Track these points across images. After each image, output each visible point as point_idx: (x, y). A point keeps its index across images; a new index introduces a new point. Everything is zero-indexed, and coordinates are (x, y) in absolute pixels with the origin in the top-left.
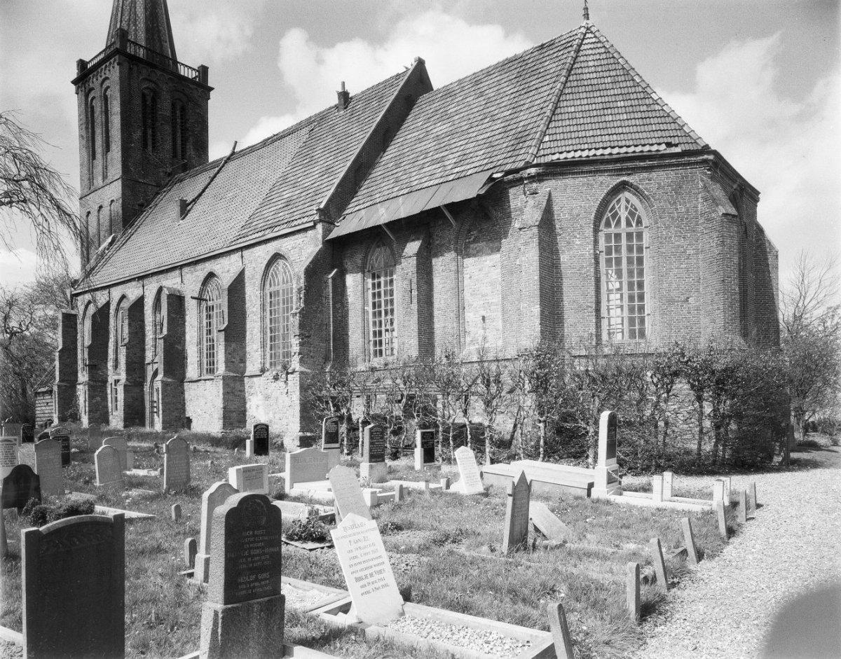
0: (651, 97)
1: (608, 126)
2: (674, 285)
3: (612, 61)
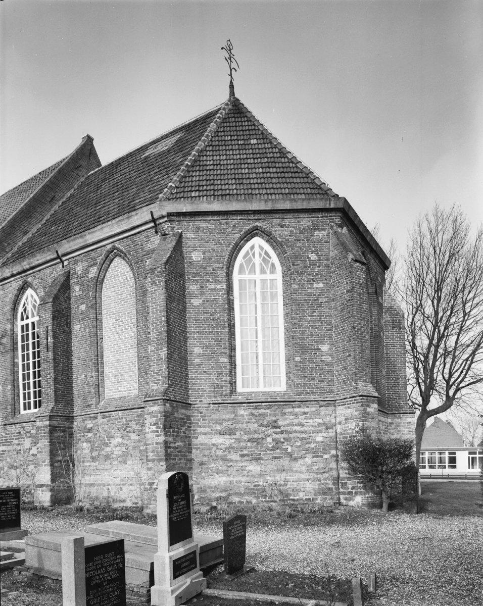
2: (307, 333)
3: (253, 127)
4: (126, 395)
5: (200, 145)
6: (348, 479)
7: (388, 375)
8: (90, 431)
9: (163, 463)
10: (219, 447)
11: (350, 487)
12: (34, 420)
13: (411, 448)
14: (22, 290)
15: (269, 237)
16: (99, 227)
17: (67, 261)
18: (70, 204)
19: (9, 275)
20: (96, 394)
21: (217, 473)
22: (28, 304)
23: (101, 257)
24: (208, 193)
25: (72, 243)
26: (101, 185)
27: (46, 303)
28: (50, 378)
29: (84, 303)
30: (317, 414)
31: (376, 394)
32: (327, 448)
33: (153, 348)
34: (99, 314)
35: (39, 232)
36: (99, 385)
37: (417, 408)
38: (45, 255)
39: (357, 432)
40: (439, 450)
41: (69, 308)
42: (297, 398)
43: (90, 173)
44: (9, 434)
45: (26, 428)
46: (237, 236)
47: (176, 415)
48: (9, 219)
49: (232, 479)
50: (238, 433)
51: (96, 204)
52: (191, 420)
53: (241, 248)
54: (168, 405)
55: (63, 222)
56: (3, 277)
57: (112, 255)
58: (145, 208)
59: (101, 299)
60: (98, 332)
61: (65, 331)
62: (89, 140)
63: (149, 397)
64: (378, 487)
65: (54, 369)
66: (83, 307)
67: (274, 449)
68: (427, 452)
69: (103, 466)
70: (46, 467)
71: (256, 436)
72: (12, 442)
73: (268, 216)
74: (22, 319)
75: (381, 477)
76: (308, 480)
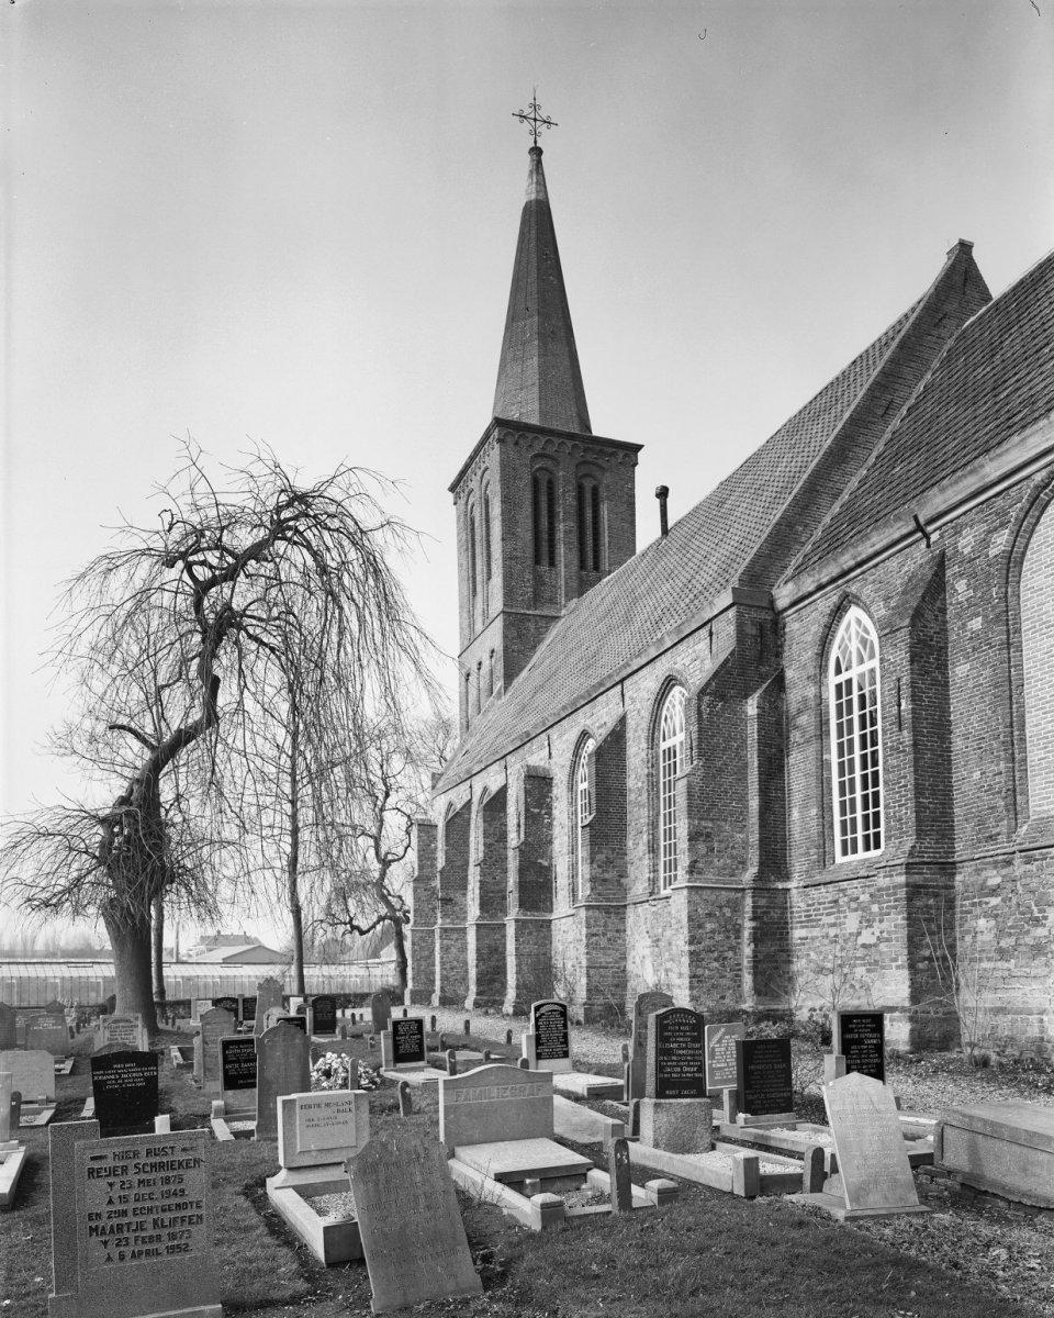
8: (994, 892)
12: (866, 875)
14: (838, 612)
16: (1016, 439)
17: (938, 532)
18: (929, 407)
19: (811, 588)
20: (1008, 810)
22: (850, 639)
23: (1019, 505)
25: (950, 492)
26: (1001, 342)
27: (897, 630)
28: (905, 786)
29: (978, 615)
34: (1014, 633)
35: (867, 485)
36: (1014, 791)
38: (888, 531)
41: (943, 631)
43: (968, 323)
44: (813, 904)
45: (849, 892)
48: (805, 476)
51: (994, 389)
55: (919, 450)
57: (1046, 494)
59: (1019, 597)
60: (1013, 673)
61: (935, 682)
62: (964, 248)
65: (915, 766)
66: (976, 624)
69: (1028, 970)
72: (820, 920)
74: (838, 671)
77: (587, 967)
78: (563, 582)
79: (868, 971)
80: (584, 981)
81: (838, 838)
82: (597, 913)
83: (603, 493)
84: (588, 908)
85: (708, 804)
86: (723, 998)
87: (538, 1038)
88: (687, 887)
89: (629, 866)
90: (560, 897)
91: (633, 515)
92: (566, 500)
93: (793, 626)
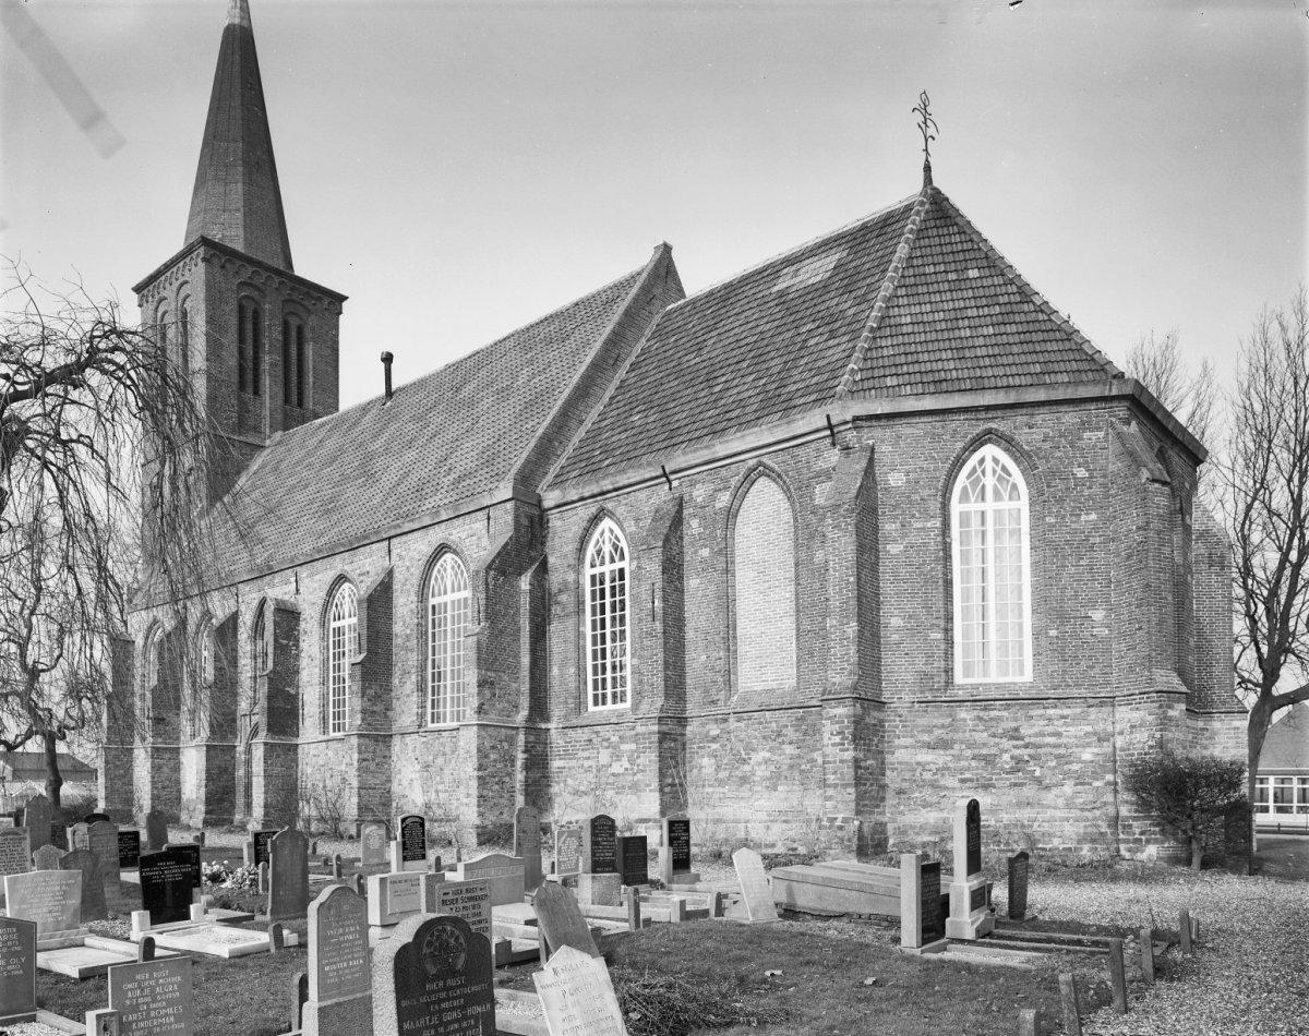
0: (1032, 301)
1: (919, 349)
2: (1069, 593)
3: (970, 245)
4: (775, 687)
5: (887, 287)
6: (1135, 819)
7: (1198, 647)
8: (714, 739)
9: (852, 790)
10: (927, 767)
11: (1138, 831)
13: (1241, 772)
14: (595, 520)
15: (1008, 443)
19: (575, 498)
21: (924, 807)
24: (913, 380)
25: (690, 456)
29: (706, 547)
30: (1083, 718)
31: (1184, 689)
32: (1099, 771)
33: (835, 622)
37: (1250, 689)
39: (1151, 747)
40: (1299, 773)
42: (1051, 694)
45: (601, 734)
46: (960, 445)
47: (867, 720)
49: (945, 815)
50: (956, 746)
52: (884, 726)
53: (964, 462)
54: (858, 705)
56: (565, 500)
58: (817, 411)
61: (676, 590)
63: (830, 693)
64: (1185, 832)
66: (705, 552)
67: (1013, 771)
68: (1272, 778)
70: (652, 794)
71: (984, 752)
73: (1009, 413)
75: (1189, 816)
76: (1067, 820)
77: (359, 788)
78: (268, 413)
79: (617, 793)
80: (355, 800)
81: (590, 692)
82: (367, 741)
83: (308, 334)
84: (360, 736)
85: (491, 659)
86: (502, 813)
87: (404, 843)
88: (477, 724)
89: (394, 701)
90: (308, 722)
91: (337, 360)
92: (272, 335)
93: (555, 522)
